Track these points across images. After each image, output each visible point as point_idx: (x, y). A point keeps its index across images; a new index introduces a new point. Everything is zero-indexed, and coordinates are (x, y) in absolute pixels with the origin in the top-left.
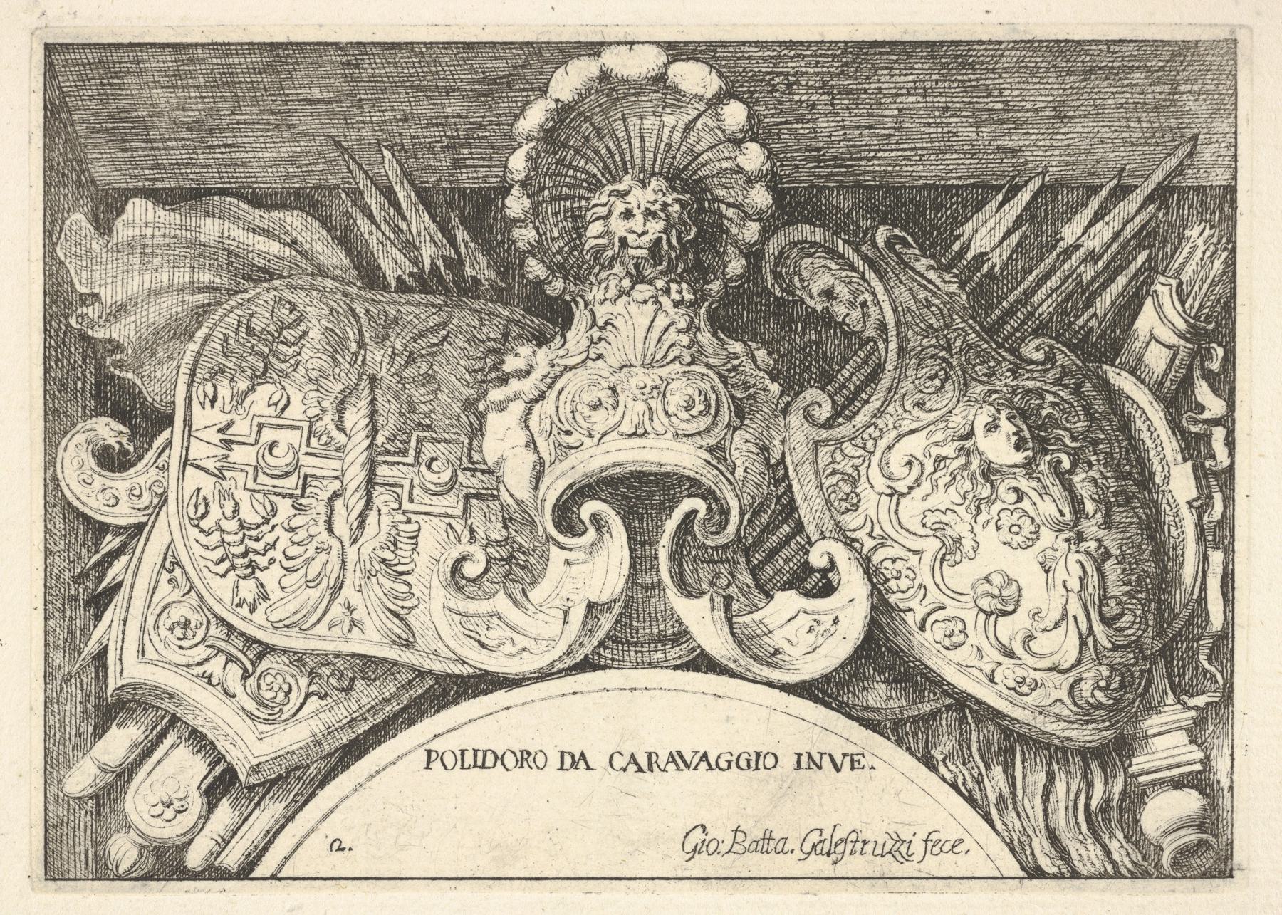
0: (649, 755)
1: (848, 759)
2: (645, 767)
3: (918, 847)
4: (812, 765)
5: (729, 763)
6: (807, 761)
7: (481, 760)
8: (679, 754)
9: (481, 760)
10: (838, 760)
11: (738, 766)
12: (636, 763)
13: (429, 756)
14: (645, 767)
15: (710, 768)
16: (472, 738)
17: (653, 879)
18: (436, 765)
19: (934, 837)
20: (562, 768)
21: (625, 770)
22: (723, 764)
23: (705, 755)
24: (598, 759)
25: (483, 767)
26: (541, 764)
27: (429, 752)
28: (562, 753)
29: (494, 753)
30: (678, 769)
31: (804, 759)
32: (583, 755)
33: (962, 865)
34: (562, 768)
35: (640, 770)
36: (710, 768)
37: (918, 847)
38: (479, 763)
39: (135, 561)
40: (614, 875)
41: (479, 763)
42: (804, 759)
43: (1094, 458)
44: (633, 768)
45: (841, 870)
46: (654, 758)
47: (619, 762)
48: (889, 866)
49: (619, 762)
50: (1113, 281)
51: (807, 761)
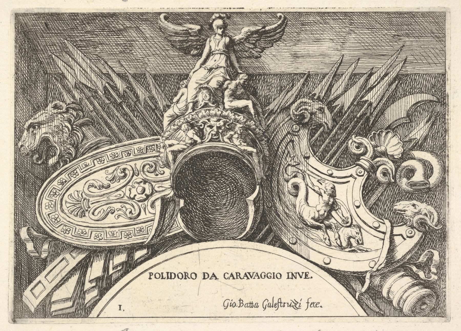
0: (237, 273)
1: (304, 274)
2: (235, 277)
4: (293, 277)
5: (265, 276)
6: (292, 276)
7: (170, 276)
9: (170, 276)
10: (301, 274)
11: (277, 278)
12: (258, 276)
14: (235, 277)
15: (259, 278)
16: (163, 269)
18: (153, 277)
19: (310, 301)
20: (288, 278)
22: (263, 277)
24: (220, 275)
25: (171, 278)
26: (194, 277)
28: (204, 273)
30: (248, 278)
31: (304, 276)
36: (259, 278)
38: (169, 277)
41: (169, 277)
42: (290, 275)
44: (231, 278)
46: (238, 274)
47: (227, 276)
48: (290, 311)
50: (294, 103)
51: (292, 276)
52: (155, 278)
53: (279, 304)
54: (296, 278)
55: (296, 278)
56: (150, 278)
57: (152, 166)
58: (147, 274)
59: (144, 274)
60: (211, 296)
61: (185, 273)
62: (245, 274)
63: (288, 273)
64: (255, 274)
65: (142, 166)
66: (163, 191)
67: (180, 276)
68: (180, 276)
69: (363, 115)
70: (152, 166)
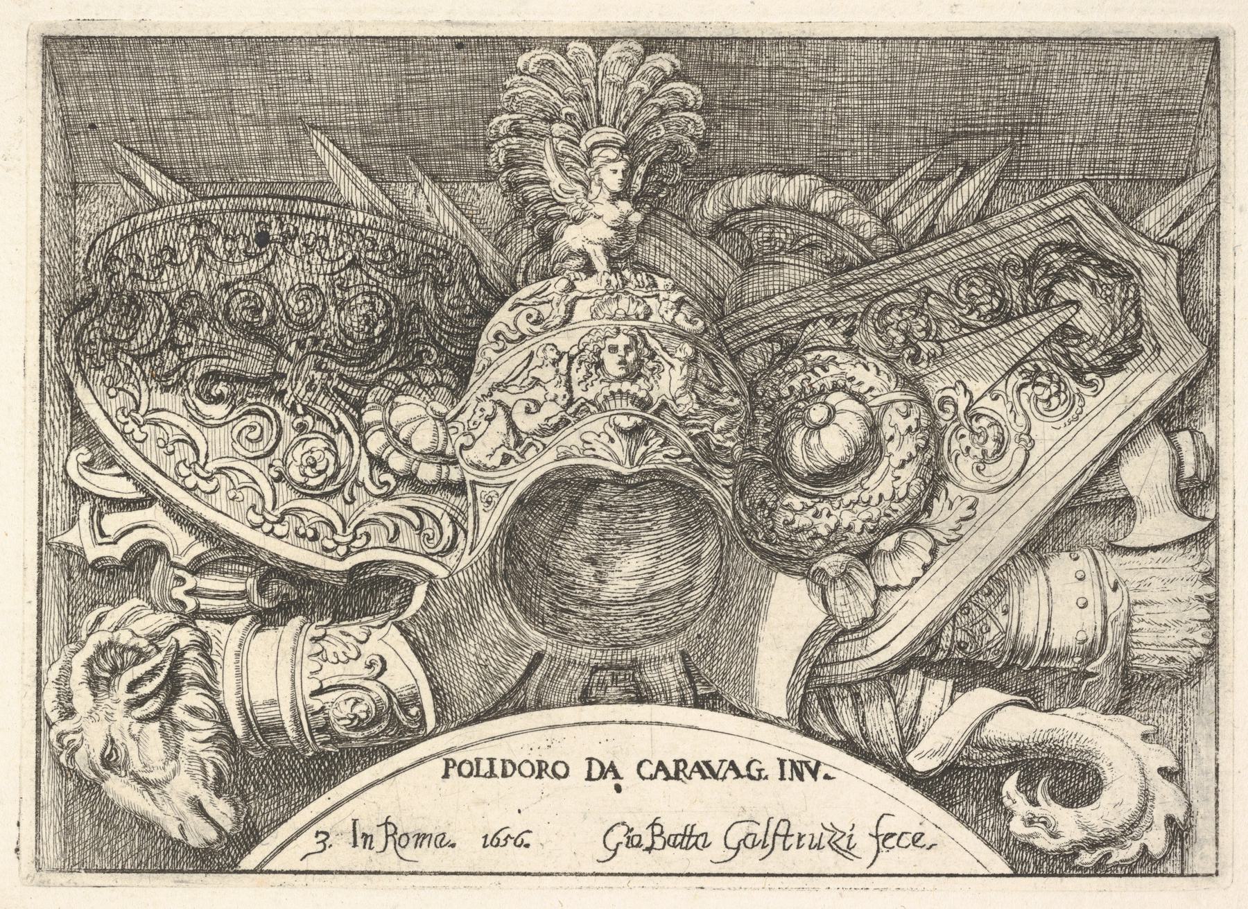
0: (677, 762)
3: (865, 846)
8: (707, 763)
13: (590, 764)
17: (455, 873)
20: (589, 778)
21: (655, 777)
23: (661, 763)
27: (447, 761)
29: (511, 762)
32: (612, 766)
33: (928, 861)
34: (589, 778)
35: (739, 775)
37: (865, 846)
39: (1072, 434)
40: (622, 871)
43: (624, 302)
45: (771, 866)
48: (827, 860)
49: (648, 770)
52: (460, 774)
53: (779, 840)
54: (801, 779)
55: (801, 779)
56: (446, 776)
57: (255, 428)
58: (439, 764)
59: (428, 764)
60: (568, 818)
61: (540, 762)
62: (697, 764)
63: (590, 760)
64: (726, 765)
65: (1042, 418)
66: (401, 517)
67: (527, 769)
68: (527, 769)
69: (1035, 191)
70: (255, 428)
